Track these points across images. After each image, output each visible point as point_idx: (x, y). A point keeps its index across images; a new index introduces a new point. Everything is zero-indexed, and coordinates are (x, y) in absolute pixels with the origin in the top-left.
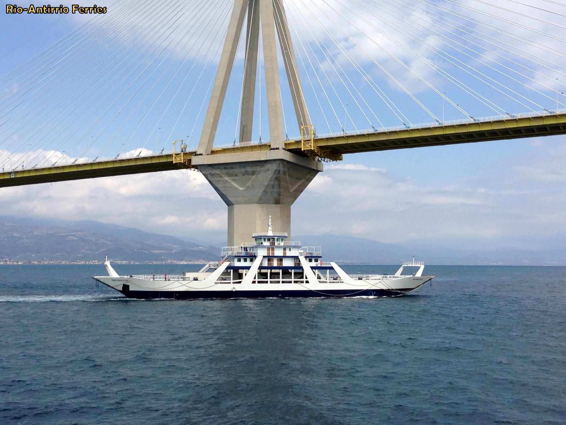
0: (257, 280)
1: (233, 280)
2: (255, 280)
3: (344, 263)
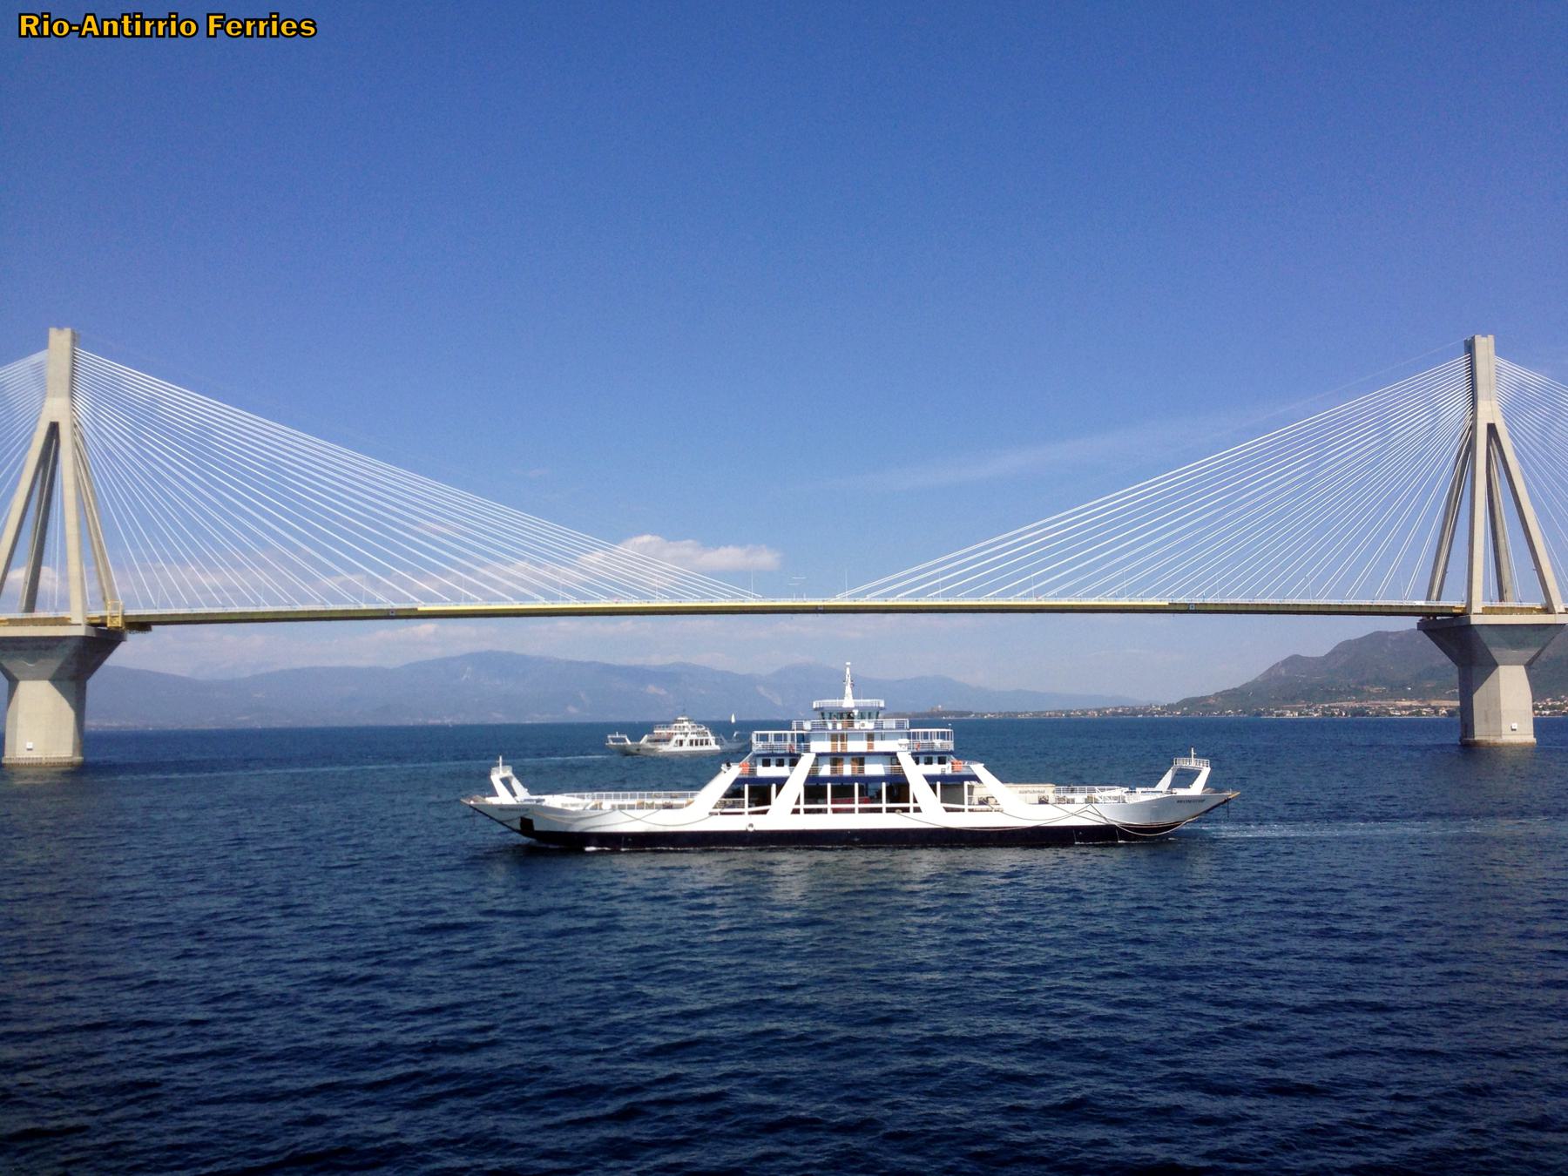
0: (802, 806)
1: (963, 803)
2: (797, 807)
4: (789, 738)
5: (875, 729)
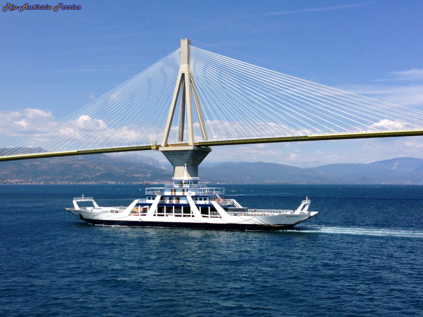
0: (157, 213)
1: (208, 214)
2: (155, 214)
3: (271, 183)
4: (202, 190)
5: (190, 188)
